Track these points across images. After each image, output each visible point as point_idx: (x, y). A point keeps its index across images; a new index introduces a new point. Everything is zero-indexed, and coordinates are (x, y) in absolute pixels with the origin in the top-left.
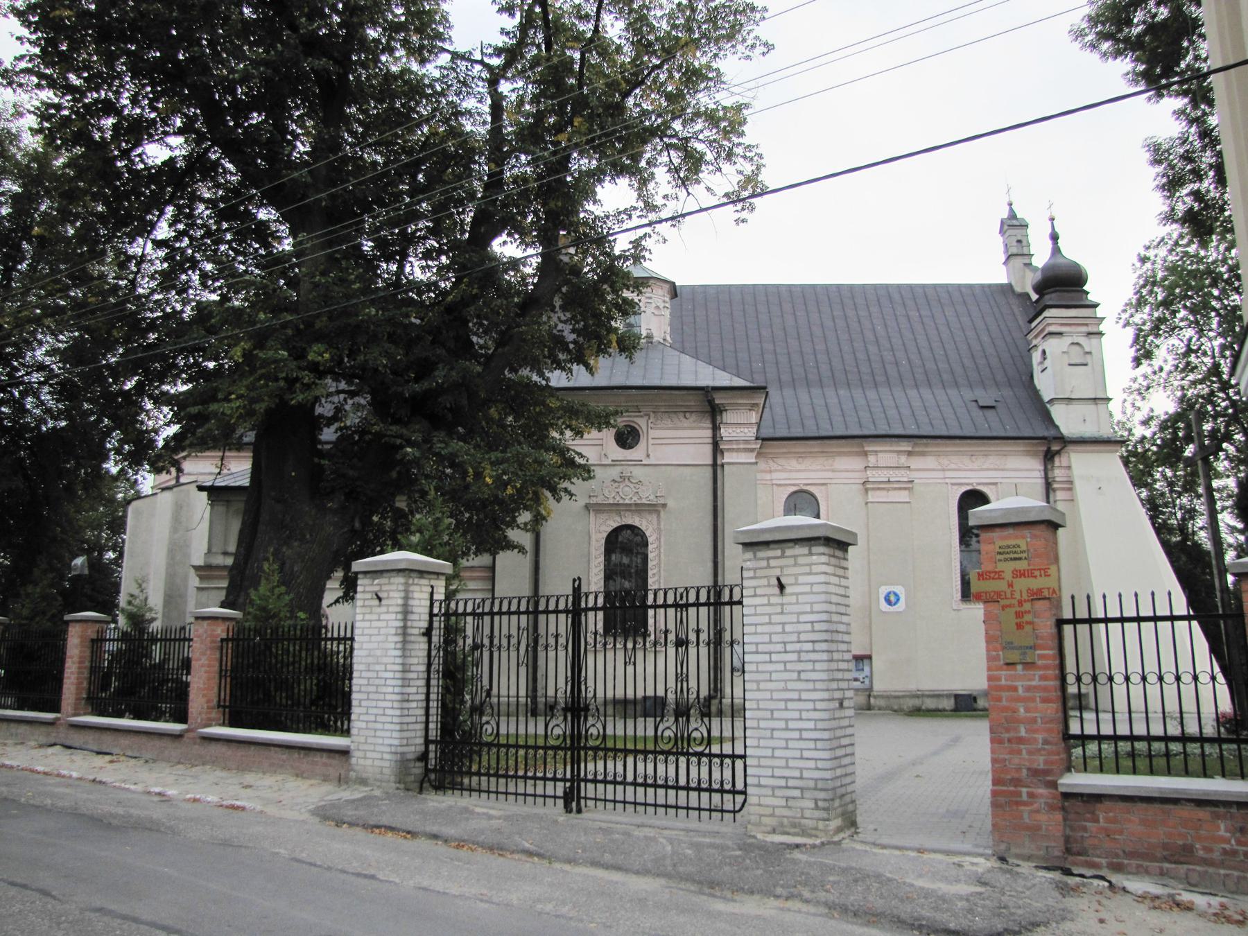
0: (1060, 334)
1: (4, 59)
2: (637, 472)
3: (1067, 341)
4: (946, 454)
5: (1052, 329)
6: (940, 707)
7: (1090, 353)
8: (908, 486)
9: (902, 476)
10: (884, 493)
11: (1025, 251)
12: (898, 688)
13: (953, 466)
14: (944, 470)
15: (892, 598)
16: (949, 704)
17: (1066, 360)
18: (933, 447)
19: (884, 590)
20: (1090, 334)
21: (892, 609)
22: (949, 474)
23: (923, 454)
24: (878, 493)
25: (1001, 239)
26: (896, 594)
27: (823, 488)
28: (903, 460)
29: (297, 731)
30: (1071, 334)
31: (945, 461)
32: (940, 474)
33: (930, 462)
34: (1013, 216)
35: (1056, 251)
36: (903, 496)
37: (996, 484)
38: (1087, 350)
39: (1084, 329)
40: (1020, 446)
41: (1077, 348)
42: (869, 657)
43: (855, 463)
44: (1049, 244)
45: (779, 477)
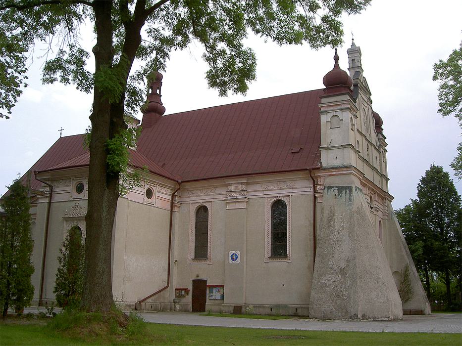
1: (367, 12)
4: (266, 182)
8: (247, 201)
9: (244, 194)
12: (38, 294)
13: (269, 188)
14: (263, 191)
15: (234, 257)
18: (161, 178)
19: (231, 253)
21: (234, 262)
23: (254, 183)
24: (231, 204)
25: (361, 58)
28: (244, 187)
30: (332, 111)
31: (265, 186)
32: (262, 193)
33: (258, 187)
34: (353, 44)
35: (337, 65)
36: (244, 205)
39: (339, 107)
40: (300, 175)
41: (336, 118)
42: (223, 287)
43: (223, 190)
45: (192, 199)
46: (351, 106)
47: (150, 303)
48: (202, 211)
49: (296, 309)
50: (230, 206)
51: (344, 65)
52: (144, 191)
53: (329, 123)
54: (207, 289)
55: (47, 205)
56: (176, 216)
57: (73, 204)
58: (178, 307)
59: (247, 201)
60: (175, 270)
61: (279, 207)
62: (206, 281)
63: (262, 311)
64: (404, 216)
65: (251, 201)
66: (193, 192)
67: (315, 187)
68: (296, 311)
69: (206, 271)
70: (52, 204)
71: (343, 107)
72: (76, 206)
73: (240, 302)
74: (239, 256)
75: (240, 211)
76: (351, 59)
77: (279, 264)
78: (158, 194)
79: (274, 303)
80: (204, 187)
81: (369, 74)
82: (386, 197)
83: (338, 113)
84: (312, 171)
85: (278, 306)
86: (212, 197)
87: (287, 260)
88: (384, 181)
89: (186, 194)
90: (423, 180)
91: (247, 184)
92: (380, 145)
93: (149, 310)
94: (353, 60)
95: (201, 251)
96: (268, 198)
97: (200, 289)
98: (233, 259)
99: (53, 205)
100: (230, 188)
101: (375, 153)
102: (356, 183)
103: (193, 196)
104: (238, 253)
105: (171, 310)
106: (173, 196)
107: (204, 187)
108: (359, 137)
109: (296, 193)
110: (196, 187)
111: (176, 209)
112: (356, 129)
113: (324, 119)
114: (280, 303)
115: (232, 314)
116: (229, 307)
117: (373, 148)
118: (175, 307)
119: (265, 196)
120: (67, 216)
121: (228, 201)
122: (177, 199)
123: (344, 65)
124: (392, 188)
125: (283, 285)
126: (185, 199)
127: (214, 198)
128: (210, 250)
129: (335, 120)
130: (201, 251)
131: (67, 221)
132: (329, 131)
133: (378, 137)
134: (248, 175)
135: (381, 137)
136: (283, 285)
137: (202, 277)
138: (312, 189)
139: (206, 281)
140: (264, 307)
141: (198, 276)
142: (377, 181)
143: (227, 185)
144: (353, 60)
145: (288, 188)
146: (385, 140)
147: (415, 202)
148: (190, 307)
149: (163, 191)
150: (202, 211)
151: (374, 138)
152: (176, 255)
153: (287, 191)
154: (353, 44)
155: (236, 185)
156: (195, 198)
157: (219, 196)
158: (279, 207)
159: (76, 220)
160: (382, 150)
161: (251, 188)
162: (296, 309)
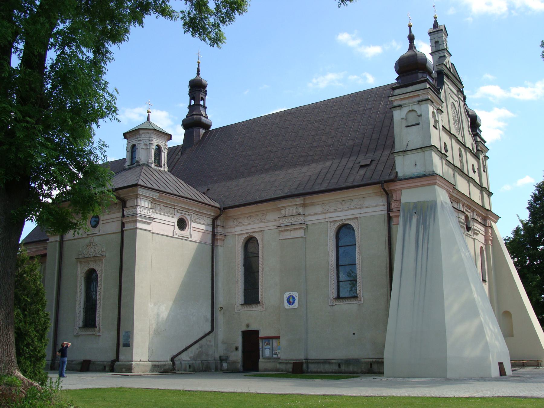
0: (400, 106)
2: (96, 239)
3: (405, 110)
5: (395, 104)
6: (319, 370)
7: (420, 115)
9: (301, 219)
10: (288, 233)
11: (441, 47)
13: (332, 210)
14: (324, 213)
15: (291, 300)
16: (290, 367)
17: (404, 124)
19: (287, 295)
20: (419, 102)
21: (291, 307)
22: (328, 215)
23: (313, 204)
24: (286, 233)
26: (293, 297)
27: (260, 233)
28: (300, 210)
29: (423, 398)
30: (407, 105)
33: (318, 209)
34: (436, 25)
35: (412, 46)
36: (300, 233)
37: (357, 218)
38: (419, 114)
41: (414, 113)
44: (408, 42)
45: (238, 229)
46: (432, 97)
47: (186, 362)
48: (250, 243)
49: (371, 365)
50: (287, 235)
51: (424, 48)
52: (175, 220)
53: (404, 121)
54: (260, 343)
55: (58, 245)
56: (220, 251)
57: (87, 241)
58: (225, 365)
59: (305, 227)
60: (221, 319)
61: (344, 231)
62: (257, 332)
63: (327, 367)
64: (516, 246)
65: (309, 227)
66: (240, 220)
67: (389, 204)
68: (340, 367)
69: (255, 318)
70: (64, 242)
71: (421, 98)
72: (91, 243)
73: (82, 358)
74: (297, 299)
75: (294, 240)
76: (434, 41)
77: (348, 307)
78: (193, 225)
79: (342, 358)
80: (252, 212)
81: (456, 59)
82: (487, 217)
83: (416, 107)
84: (386, 183)
85: (348, 362)
86: (262, 225)
87: (357, 302)
88: (485, 196)
89: (231, 223)
90: (536, 198)
91: (304, 205)
92: (478, 150)
93: (185, 371)
94: (437, 42)
95: (251, 295)
96: (331, 222)
97: (251, 339)
98: (290, 303)
99: (66, 245)
100: (283, 212)
101: (472, 161)
102: (442, 196)
103: (240, 226)
104: (295, 294)
105: (216, 370)
106: (214, 226)
107: (252, 212)
108: (446, 138)
109: (365, 210)
110: (242, 214)
111: (219, 243)
112: (441, 127)
113: (398, 115)
114: (350, 357)
115: (290, 372)
116: (286, 364)
117: (468, 154)
118: (222, 365)
119: (327, 220)
120: (81, 256)
121: (282, 229)
122: (220, 230)
123: (424, 48)
124: (496, 205)
125: (354, 334)
126: (229, 230)
127: (262, 225)
128: (262, 292)
129: (412, 116)
130: (251, 295)
131: (81, 263)
132: (405, 130)
133: (476, 141)
134: (305, 193)
135: (479, 139)
136: (354, 334)
137: (253, 328)
138: (386, 208)
139: (257, 332)
140: (332, 363)
141: (248, 326)
142: (475, 195)
143: (279, 209)
144: (437, 42)
145: (356, 208)
146: (486, 144)
147: (525, 225)
148: (240, 366)
149: (200, 221)
150: (250, 243)
151: (469, 141)
152: (221, 300)
153: (353, 212)
154: (436, 25)
155: (290, 207)
156: (240, 228)
157: (271, 224)
158: (344, 231)
159: (92, 261)
160: (481, 157)
161: (310, 210)
162: (371, 365)
